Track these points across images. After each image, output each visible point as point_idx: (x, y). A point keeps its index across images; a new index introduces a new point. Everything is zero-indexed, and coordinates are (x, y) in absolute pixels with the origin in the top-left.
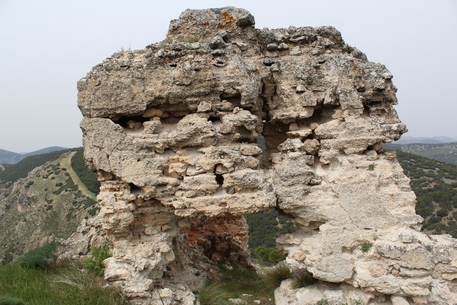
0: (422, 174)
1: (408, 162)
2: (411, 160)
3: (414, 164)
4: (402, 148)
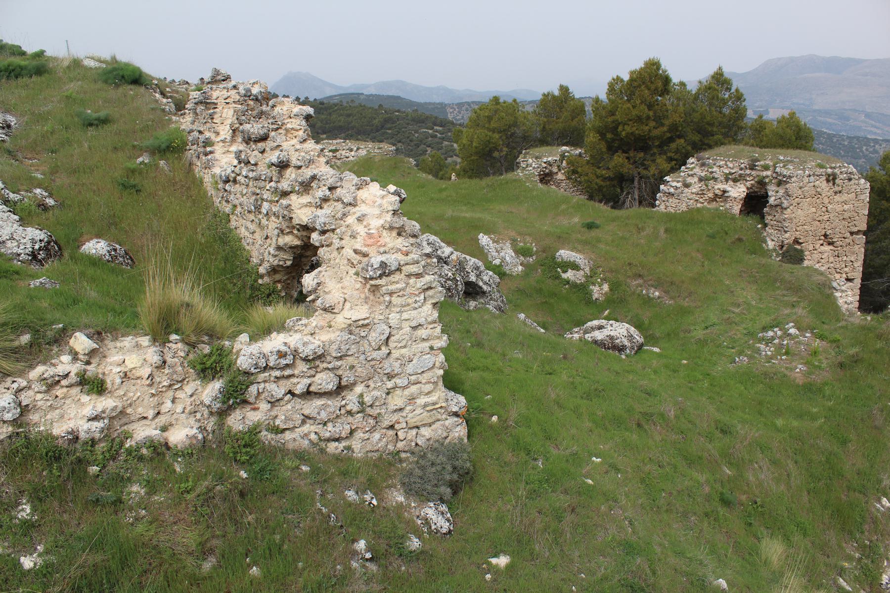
0: (451, 154)
1: (430, 131)
2: (435, 128)
3: (439, 135)
4: (449, 110)
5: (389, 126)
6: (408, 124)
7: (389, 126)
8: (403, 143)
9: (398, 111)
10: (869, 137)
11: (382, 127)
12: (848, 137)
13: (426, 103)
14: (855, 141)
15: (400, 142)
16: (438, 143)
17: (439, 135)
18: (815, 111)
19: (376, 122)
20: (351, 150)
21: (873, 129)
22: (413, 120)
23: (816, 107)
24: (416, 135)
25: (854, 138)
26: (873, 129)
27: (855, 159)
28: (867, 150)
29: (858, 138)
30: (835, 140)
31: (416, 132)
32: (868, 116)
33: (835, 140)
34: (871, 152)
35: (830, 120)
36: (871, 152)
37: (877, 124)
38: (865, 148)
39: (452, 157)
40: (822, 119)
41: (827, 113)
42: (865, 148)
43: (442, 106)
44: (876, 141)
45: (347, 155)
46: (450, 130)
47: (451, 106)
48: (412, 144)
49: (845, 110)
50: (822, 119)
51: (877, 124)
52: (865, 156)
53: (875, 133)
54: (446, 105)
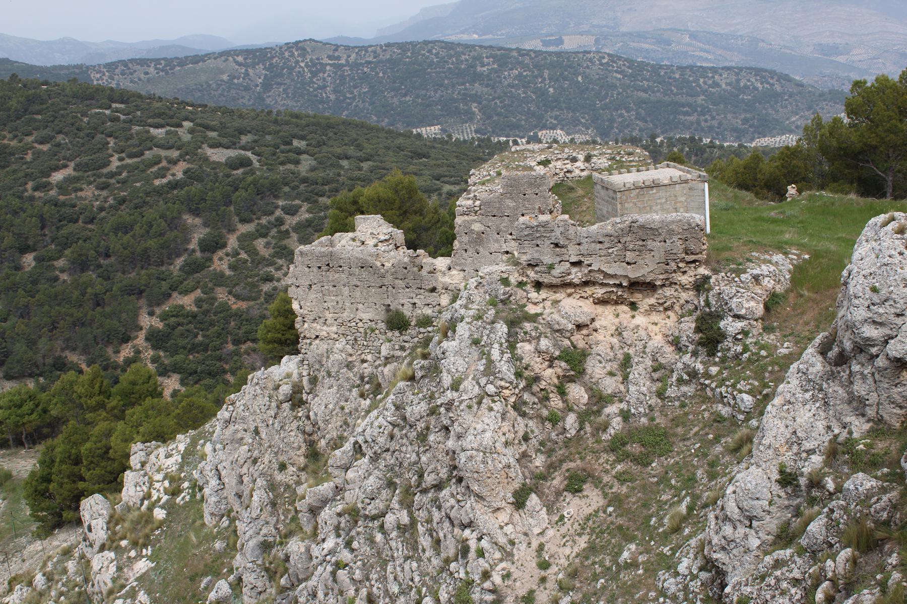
0: (149, 144)
1: (107, 112)
2: (114, 105)
3: (122, 117)
5: (36, 107)
6: (68, 103)
7: (36, 107)
8: (66, 134)
9: (46, 83)
10: (704, 65)
11: (26, 110)
12: (679, 68)
13: (55, 68)
14: (688, 72)
15: (60, 132)
16: (124, 130)
17: (122, 117)
18: (624, 35)
19: (13, 103)
20: (574, 160)
21: (702, 54)
22: (75, 96)
23: (624, 29)
24: (86, 119)
25: (687, 67)
26: (702, 54)
27: (692, 96)
28: (705, 83)
29: (691, 67)
30: (662, 73)
31: (85, 114)
32: (693, 36)
33: (662, 73)
34: (710, 86)
35: (646, 46)
36: (710, 86)
37: (707, 47)
38: (701, 80)
39: (151, 149)
40: (635, 44)
41: (641, 36)
42: (701, 80)
43: (84, 70)
44: (714, 70)
45: (569, 166)
46: (138, 108)
47: (96, 68)
48: (82, 134)
49: (664, 30)
50: (635, 44)
51: (707, 47)
52: (704, 92)
53: (706, 60)
54: (87, 67)
